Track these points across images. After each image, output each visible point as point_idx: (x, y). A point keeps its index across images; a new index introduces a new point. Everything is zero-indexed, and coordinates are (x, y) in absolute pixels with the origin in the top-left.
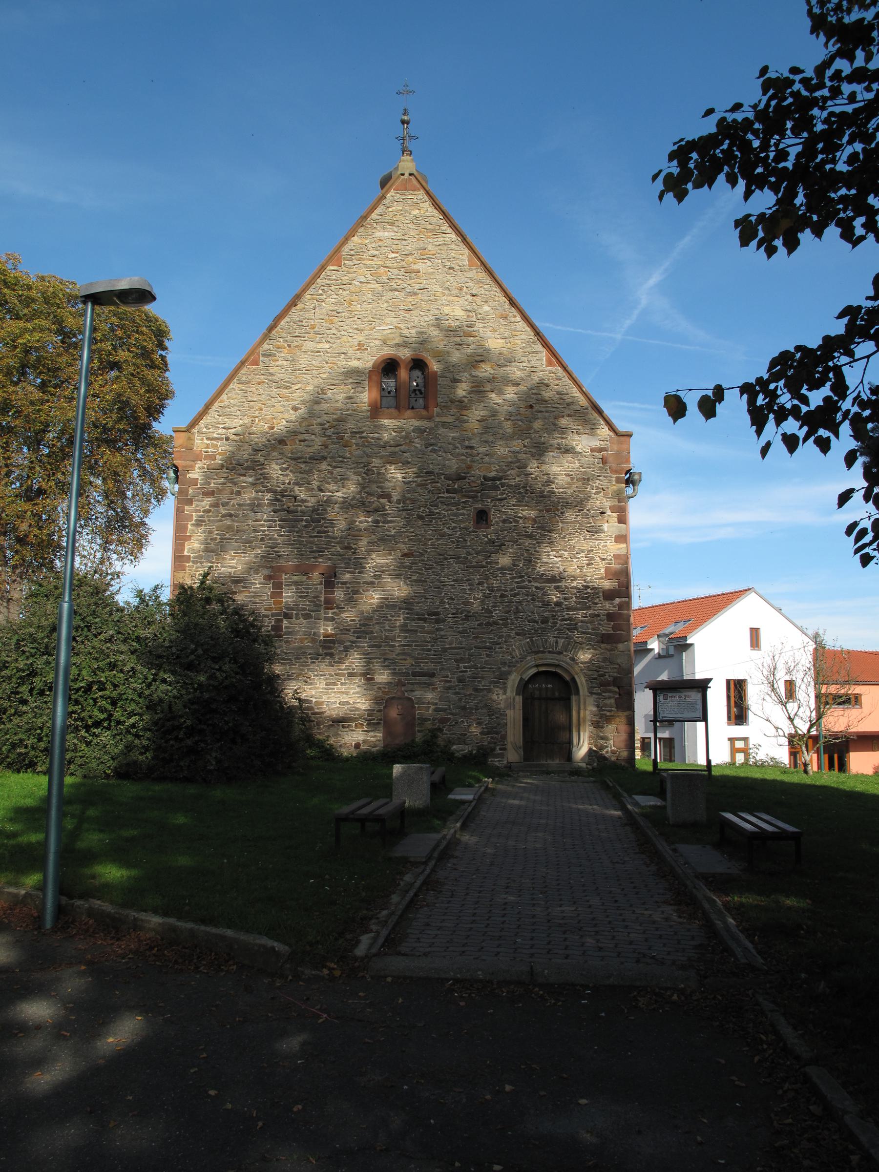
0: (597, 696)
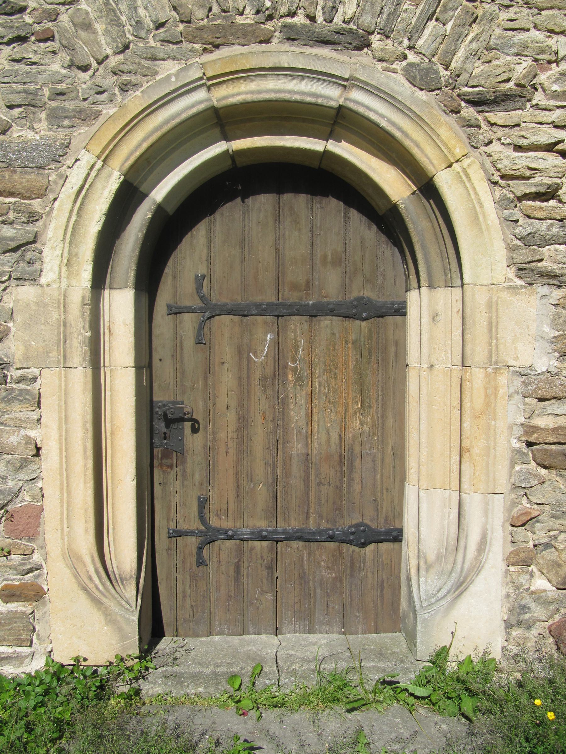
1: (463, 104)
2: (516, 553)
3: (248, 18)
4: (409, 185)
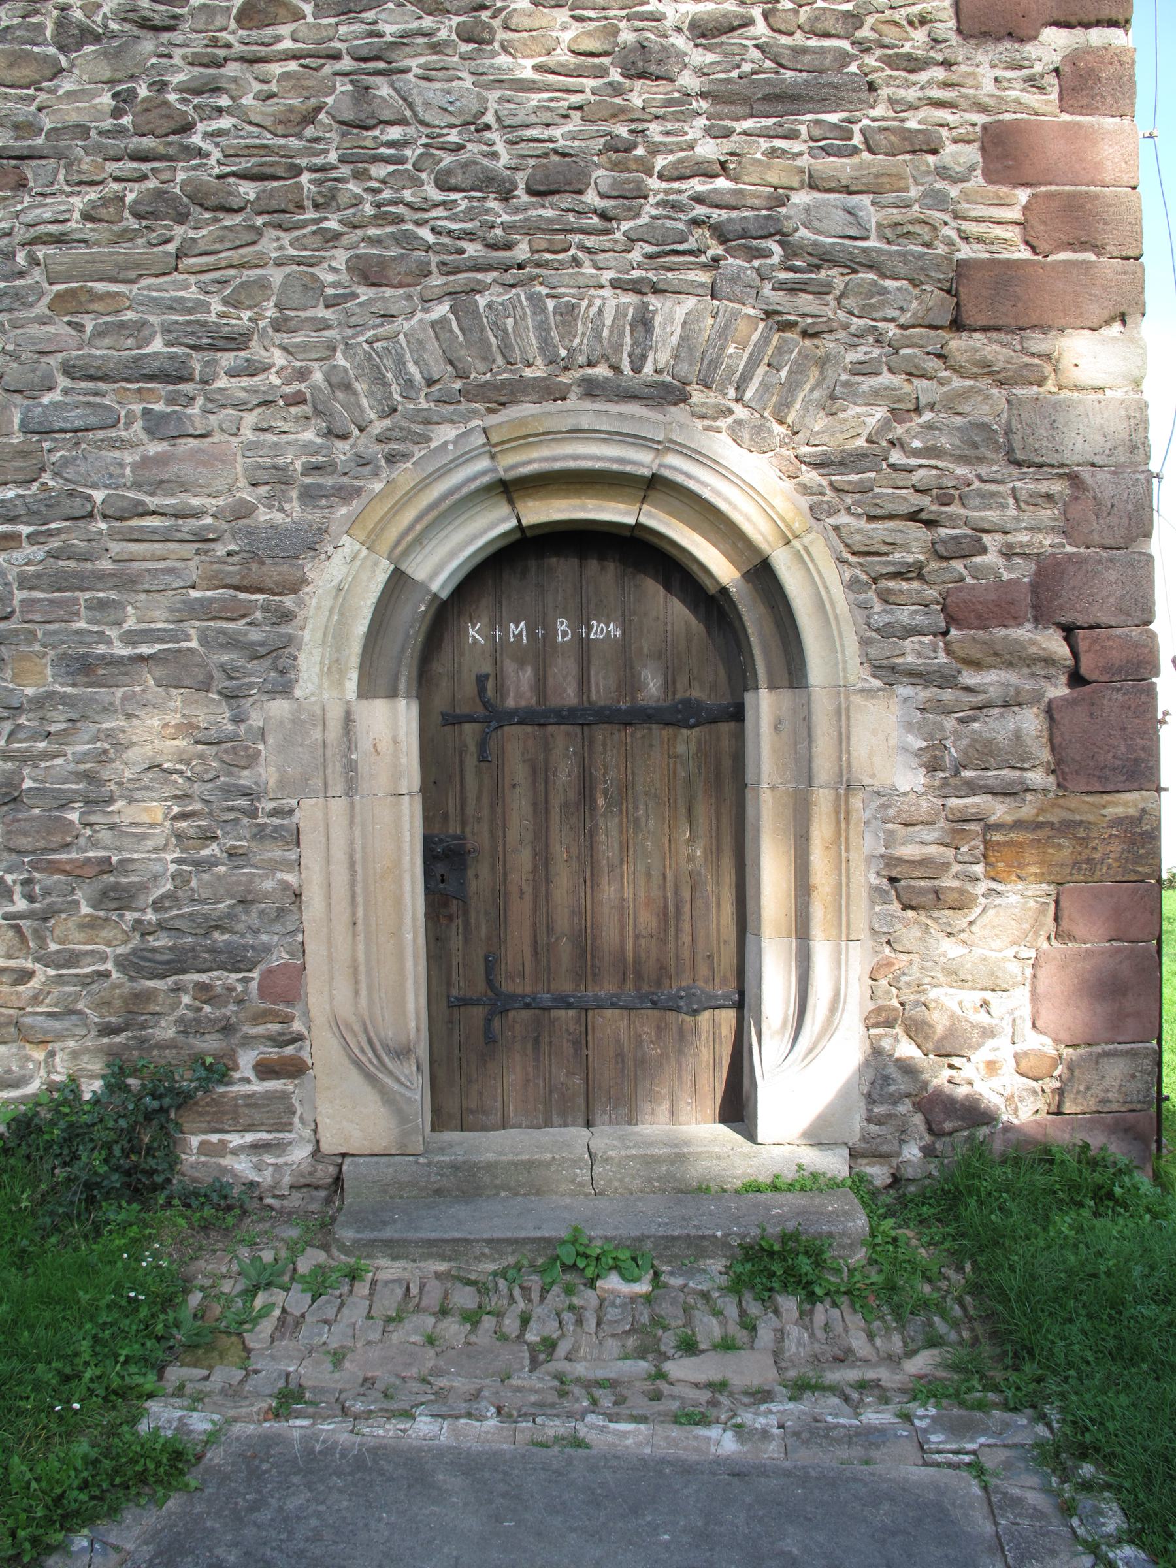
0: (924, 694)
1: (803, 467)
2: (879, 1010)
3: (538, 371)
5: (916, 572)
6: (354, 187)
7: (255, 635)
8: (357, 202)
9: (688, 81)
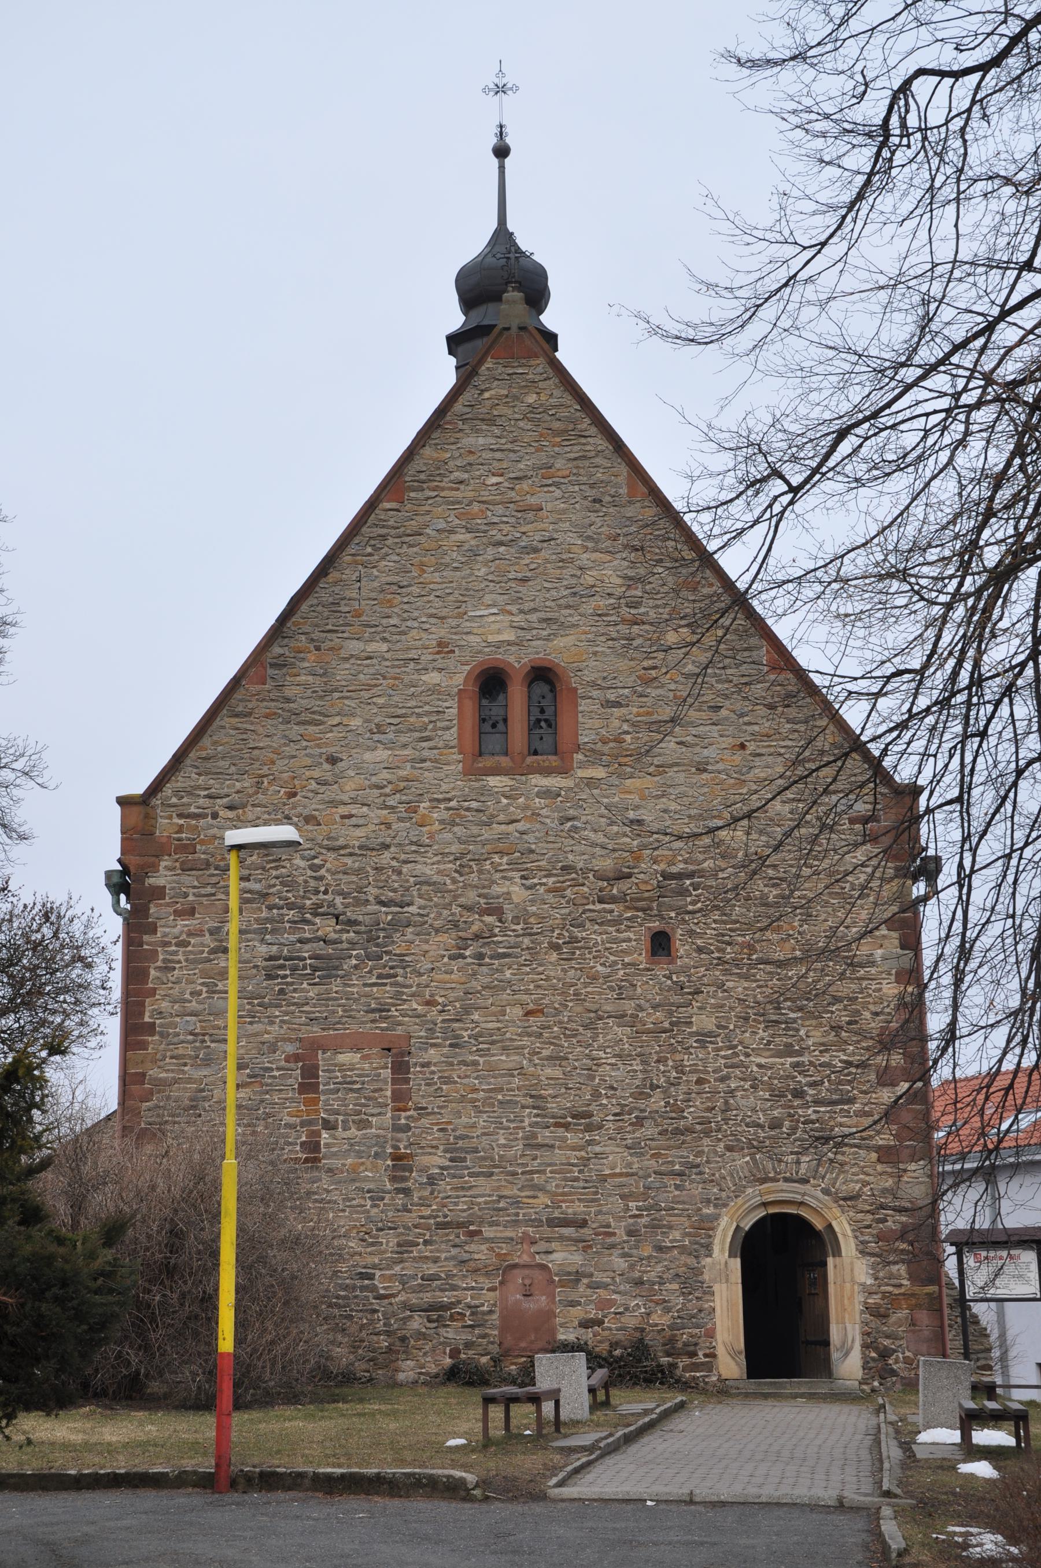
4: (798, 1383)
5: (869, 1227)
6: (725, 1127)
7: (703, 1241)
8: (726, 1131)
9: (808, 1098)
